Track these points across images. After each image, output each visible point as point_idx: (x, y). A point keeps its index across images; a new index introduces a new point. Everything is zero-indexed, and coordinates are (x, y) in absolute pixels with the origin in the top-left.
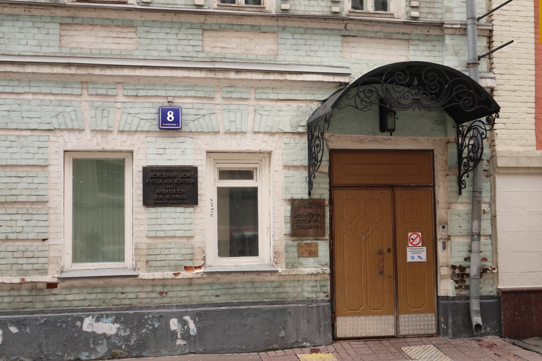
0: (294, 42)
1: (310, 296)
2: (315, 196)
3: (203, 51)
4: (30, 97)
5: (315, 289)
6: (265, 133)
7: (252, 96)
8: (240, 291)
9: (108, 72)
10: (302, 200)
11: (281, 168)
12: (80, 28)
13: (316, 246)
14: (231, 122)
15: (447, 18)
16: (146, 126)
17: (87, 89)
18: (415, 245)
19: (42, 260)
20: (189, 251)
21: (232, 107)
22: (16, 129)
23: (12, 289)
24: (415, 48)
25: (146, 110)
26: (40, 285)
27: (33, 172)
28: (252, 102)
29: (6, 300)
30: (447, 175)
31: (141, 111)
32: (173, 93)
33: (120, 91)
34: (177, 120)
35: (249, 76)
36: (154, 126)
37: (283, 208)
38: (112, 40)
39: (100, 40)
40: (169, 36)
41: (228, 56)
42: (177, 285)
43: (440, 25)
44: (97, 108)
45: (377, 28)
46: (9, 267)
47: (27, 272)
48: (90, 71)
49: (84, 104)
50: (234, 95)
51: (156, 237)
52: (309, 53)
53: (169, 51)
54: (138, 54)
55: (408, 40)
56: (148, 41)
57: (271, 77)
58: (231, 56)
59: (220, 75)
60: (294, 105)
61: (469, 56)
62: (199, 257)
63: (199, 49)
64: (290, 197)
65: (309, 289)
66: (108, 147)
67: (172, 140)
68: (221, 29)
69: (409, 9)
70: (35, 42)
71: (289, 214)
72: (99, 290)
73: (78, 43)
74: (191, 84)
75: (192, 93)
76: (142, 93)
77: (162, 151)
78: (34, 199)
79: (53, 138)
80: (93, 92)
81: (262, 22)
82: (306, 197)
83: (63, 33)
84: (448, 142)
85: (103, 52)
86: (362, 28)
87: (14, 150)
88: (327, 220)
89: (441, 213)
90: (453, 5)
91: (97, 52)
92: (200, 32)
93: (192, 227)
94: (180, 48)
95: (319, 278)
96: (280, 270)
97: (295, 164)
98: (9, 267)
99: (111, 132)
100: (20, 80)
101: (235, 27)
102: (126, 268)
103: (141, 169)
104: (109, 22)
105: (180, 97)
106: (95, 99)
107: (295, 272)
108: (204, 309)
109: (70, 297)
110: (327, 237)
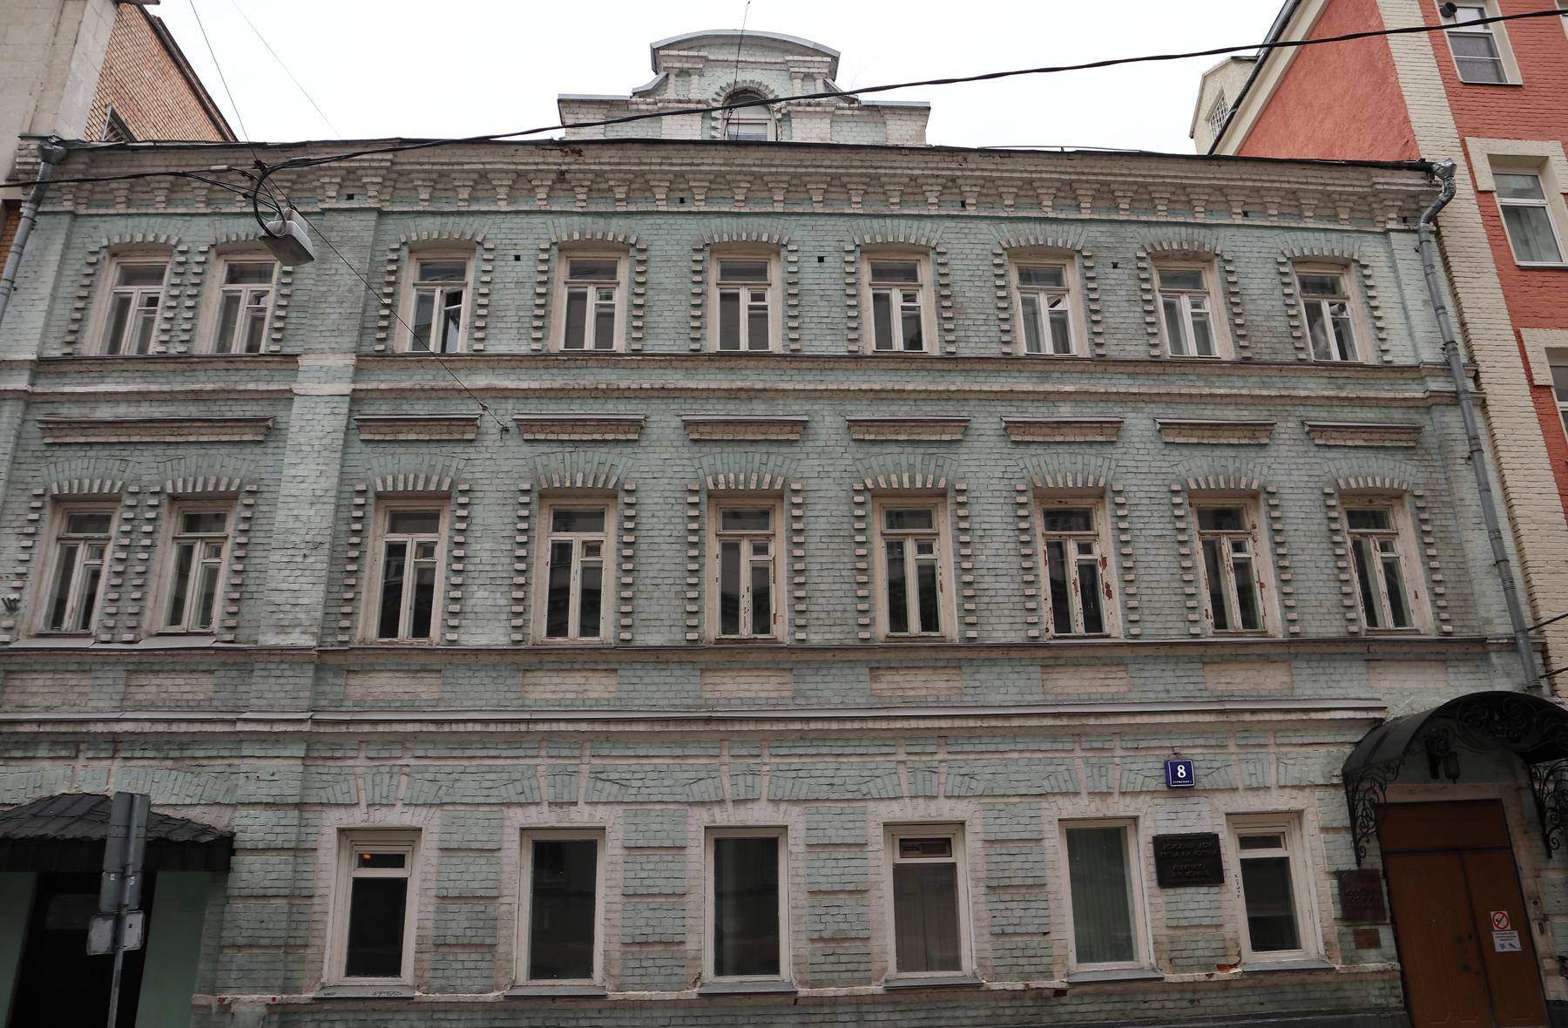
0: (1310, 671)
1: (1379, 1001)
2: (1366, 866)
3: (1206, 690)
4: (1016, 755)
5: (1384, 992)
6: (1293, 787)
7: (1272, 742)
8: (1290, 996)
9: (1105, 721)
10: (1350, 872)
11: (1317, 831)
12: (1063, 669)
13: (1377, 933)
14: (1251, 774)
15: (1488, 631)
16: (1152, 785)
17: (1080, 742)
18: (1503, 929)
19: (1046, 960)
20: (1220, 945)
21: (1250, 756)
22: (1003, 796)
23: (1014, 998)
24: (1455, 670)
25: (1150, 765)
26: (1047, 992)
27: (1027, 847)
28: (1272, 749)
29: (1008, 1012)
30: (1526, 832)
31: (1145, 766)
32: (1176, 743)
33: (1117, 744)
34: (1189, 776)
35: (1267, 717)
36: (1158, 784)
37: (1328, 884)
38: (1100, 682)
39: (1086, 683)
40: (1166, 674)
41: (1236, 693)
42: (1210, 990)
43: (1482, 642)
44: (1092, 765)
45: (1405, 649)
46: (1008, 969)
47: (1029, 976)
48: (1084, 721)
49: (1078, 761)
50: (1251, 742)
51: (1177, 927)
52: (1331, 684)
53: (1168, 691)
54: (1133, 696)
55: (1444, 661)
56: (1142, 681)
57: (1293, 716)
58: (1239, 693)
59: (1234, 718)
60: (1323, 750)
61: (1526, 677)
62: (1233, 951)
63: (1202, 687)
64: (1334, 869)
65: (1376, 993)
66: (1110, 813)
67: (1184, 801)
68: (1223, 660)
69: (1438, 623)
70: (1016, 690)
71: (1336, 891)
72: (1116, 999)
73: (1063, 688)
74: (1198, 731)
75: (1201, 741)
76: (1143, 744)
77: (1173, 816)
78: (1030, 881)
79: (1045, 805)
80: (1086, 745)
81: (1272, 650)
82: (1354, 867)
83: (1045, 676)
84: (1519, 789)
85: (1093, 696)
86: (1388, 649)
87: (1003, 821)
88: (1386, 898)
89: (1528, 883)
90: (1492, 614)
91: (1086, 697)
92: (1200, 666)
93: (1218, 913)
94: (1180, 687)
95: (1386, 976)
96: (1337, 967)
97: (1335, 824)
98: (1007, 969)
99: (1111, 794)
100: (1003, 736)
101: (1239, 658)
102: (1143, 969)
103: (1150, 839)
104: (1096, 661)
105: (1188, 747)
106: (1089, 754)
107: (1356, 968)
108: (1248, 1021)
109: (1083, 1008)
110: (1388, 921)
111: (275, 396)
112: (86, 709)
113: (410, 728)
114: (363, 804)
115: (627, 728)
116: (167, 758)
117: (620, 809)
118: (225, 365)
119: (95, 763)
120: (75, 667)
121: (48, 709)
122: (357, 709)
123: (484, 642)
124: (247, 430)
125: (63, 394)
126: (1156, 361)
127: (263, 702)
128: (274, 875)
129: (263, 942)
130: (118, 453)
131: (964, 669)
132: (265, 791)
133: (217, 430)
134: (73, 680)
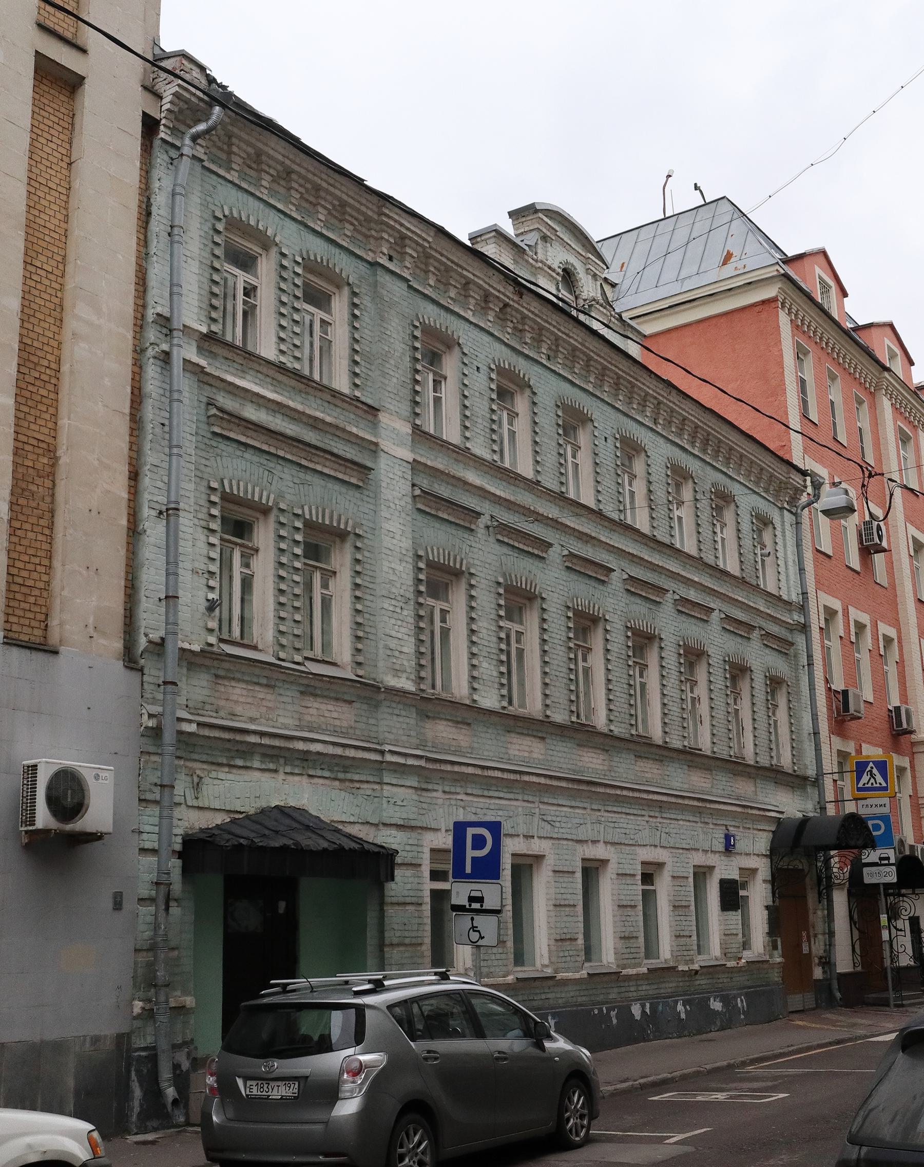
111: (364, 444)
112: (275, 724)
113: (470, 770)
114: (443, 830)
115: (680, 801)
116: (335, 779)
117: (550, 842)
118: (329, 398)
119: (290, 778)
120: (264, 681)
121: (252, 720)
122: (434, 750)
123: (489, 705)
124: (355, 473)
125: (223, 380)
126: (654, 539)
127: (391, 737)
128: (409, 886)
129: (407, 941)
130: (265, 462)
131: (547, 741)
132: (398, 815)
133: (337, 466)
134: (261, 693)
